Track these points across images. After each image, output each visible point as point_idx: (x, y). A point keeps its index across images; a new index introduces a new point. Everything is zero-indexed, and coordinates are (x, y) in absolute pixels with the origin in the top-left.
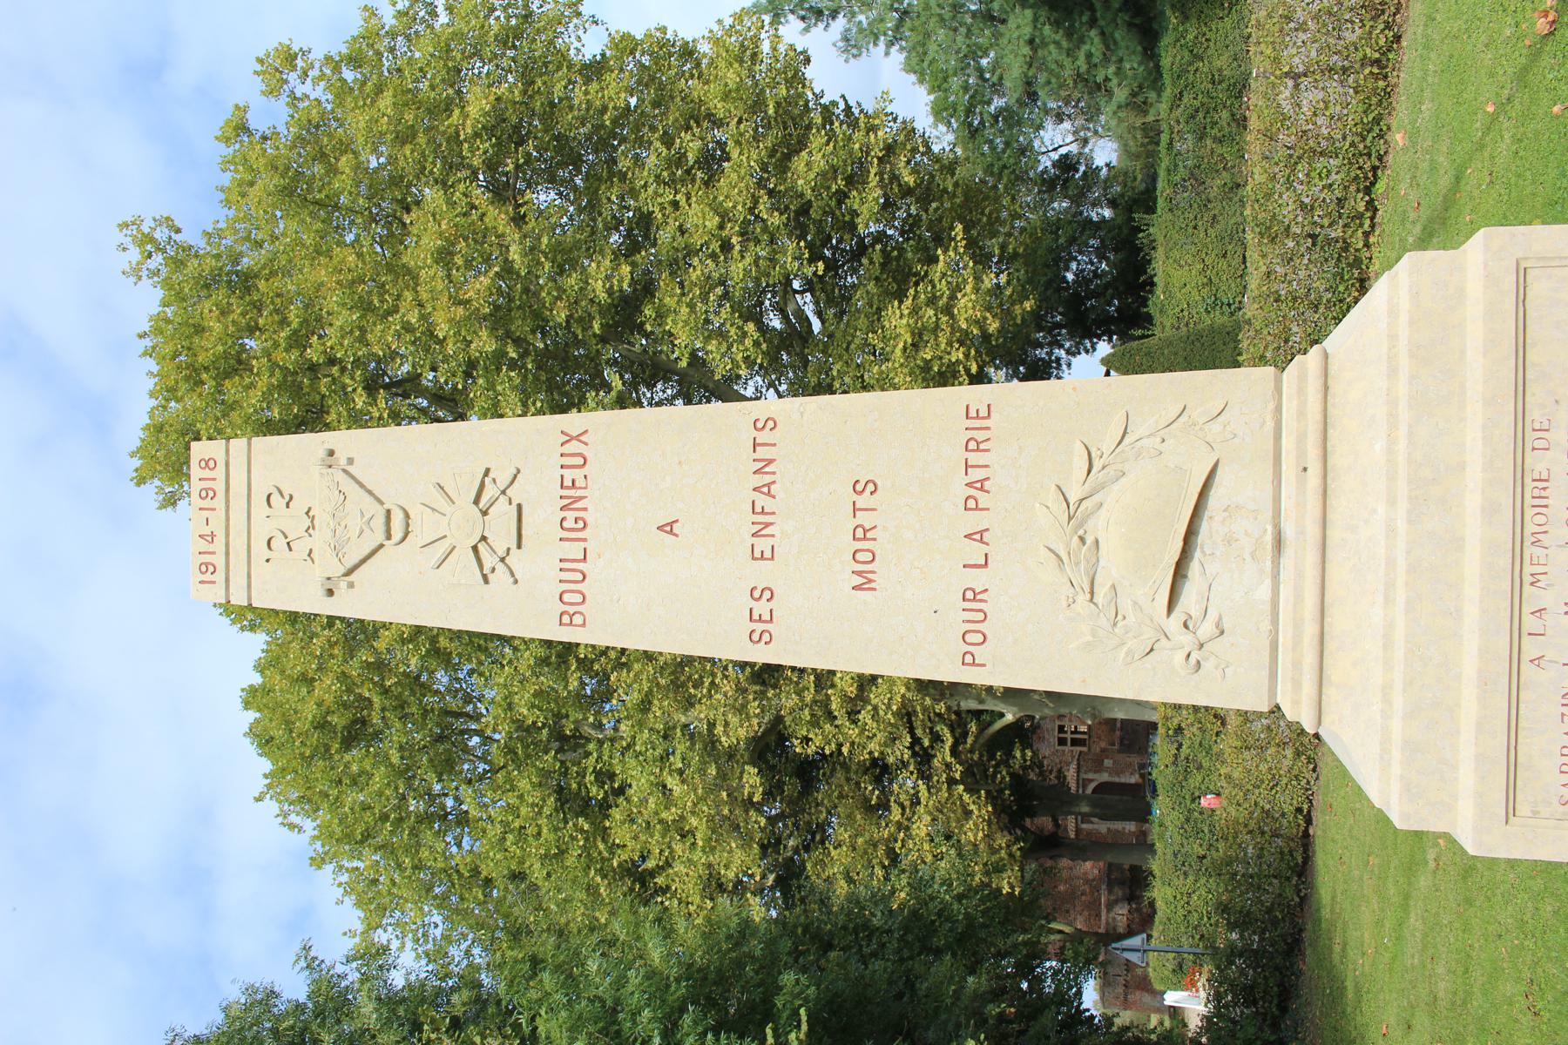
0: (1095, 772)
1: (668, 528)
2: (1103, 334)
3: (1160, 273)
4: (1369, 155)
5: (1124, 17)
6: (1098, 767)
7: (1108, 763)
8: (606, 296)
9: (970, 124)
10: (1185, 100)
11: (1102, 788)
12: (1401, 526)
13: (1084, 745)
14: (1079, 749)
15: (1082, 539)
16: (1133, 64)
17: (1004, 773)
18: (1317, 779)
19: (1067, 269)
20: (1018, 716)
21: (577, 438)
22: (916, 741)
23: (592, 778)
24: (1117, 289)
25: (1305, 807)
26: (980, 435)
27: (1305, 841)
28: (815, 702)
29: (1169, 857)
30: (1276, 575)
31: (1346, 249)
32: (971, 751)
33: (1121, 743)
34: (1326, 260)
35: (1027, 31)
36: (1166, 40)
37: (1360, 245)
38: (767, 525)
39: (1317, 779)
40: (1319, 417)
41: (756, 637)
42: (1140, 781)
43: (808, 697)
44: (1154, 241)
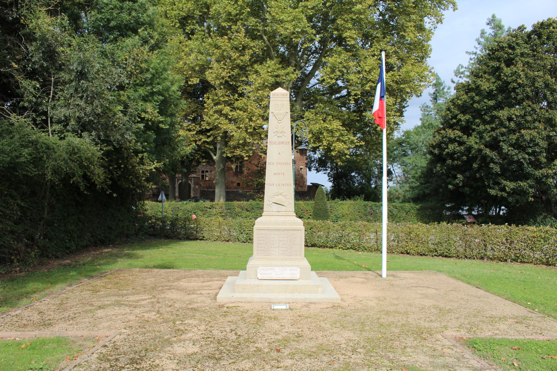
0: (194, 183)
1: (280, 154)
2: (335, 184)
3: (346, 202)
5: (422, 193)
6: (196, 184)
7: (197, 187)
8: (345, 36)
9: (403, 143)
10: (395, 210)
11: (190, 185)
14: (201, 177)
16: (408, 195)
19: (356, 173)
22: (208, 131)
23: (192, 28)
25: (205, 239)
28: (220, 100)
29: (177, 206)
32: (204, 147)
33: (203, 191)
35: (419, 165)
36: (412, 204)
42: (192, 197)
43: (221, 99)
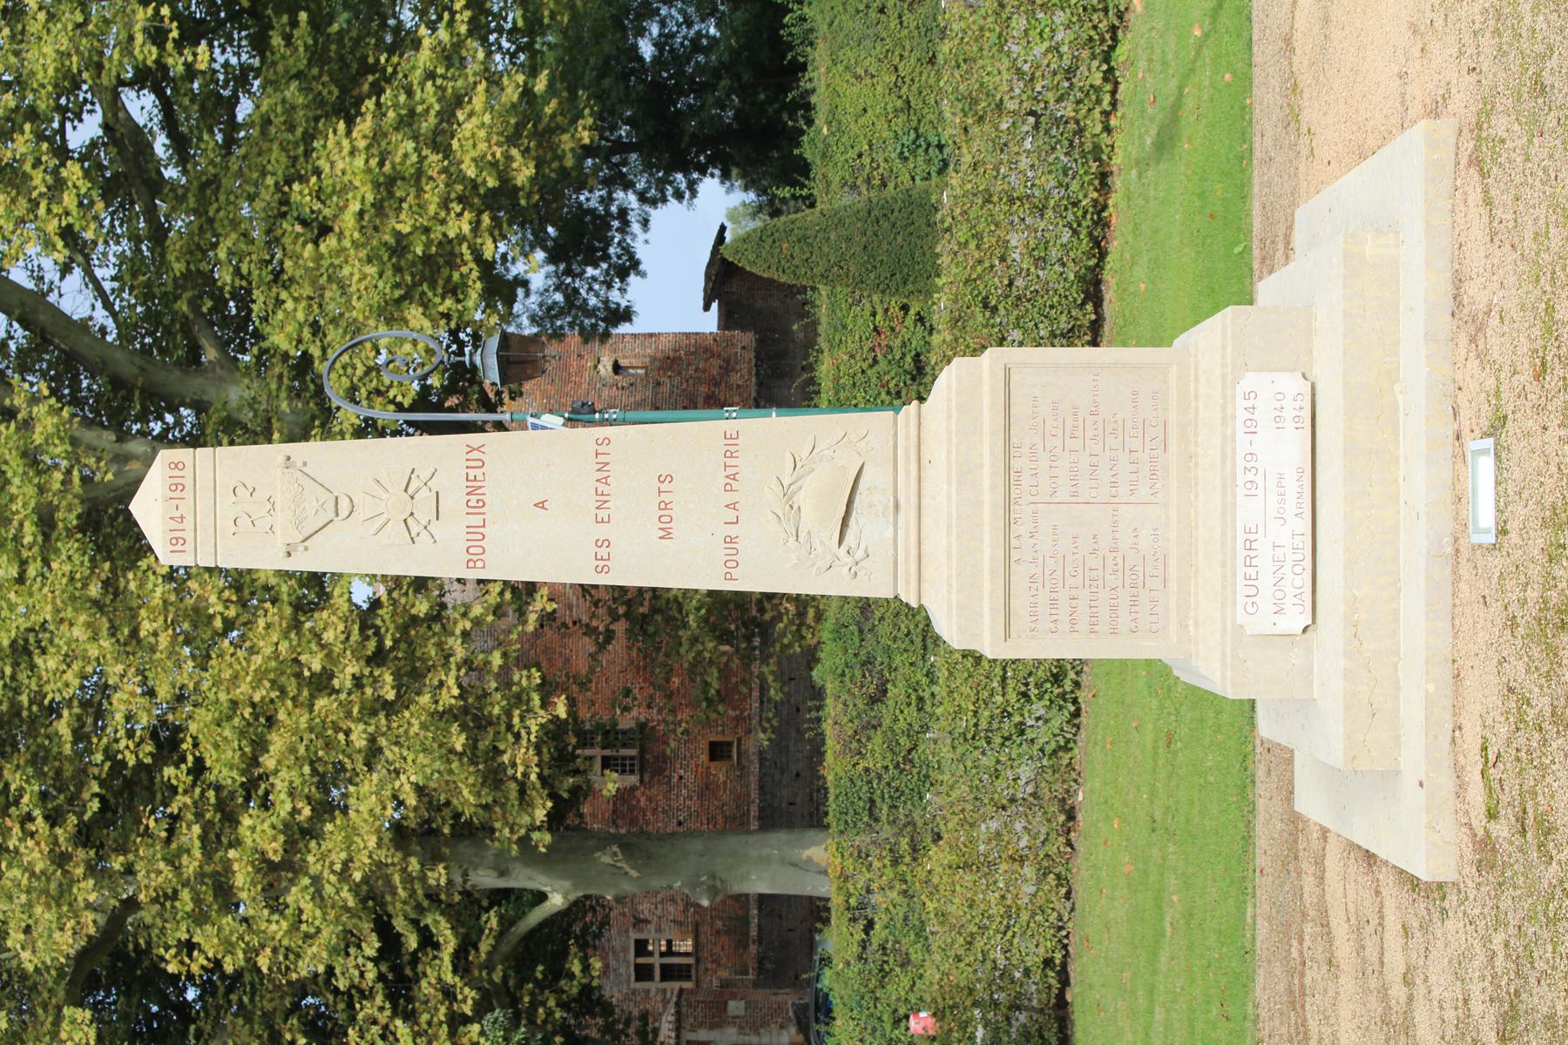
0: (712, 1027)
1: (541, 505)
2: (712, 161)
4: (1106, 10)
7: (735, 1007)
12: (954, 496)
13: (688, 978)
15: (791, 507)
17: (552, 1003)
18: (1073, 909)
19: (641, 32)
20: (572, 897)
21: (477, 449)
24: (738, 77)
26: (733, 449)
27: (1061, 1012)
28: (201, 875)
30: (895, 524)
31: (1080, 131)
33: (760, 969)
34: (1053, 149)
37: (1098, 128)
38: (605, 502)
39: (1073, 909)
40: (916, 439)
41: (599, 569)
43: (190, 865)
44: (812, 30)
